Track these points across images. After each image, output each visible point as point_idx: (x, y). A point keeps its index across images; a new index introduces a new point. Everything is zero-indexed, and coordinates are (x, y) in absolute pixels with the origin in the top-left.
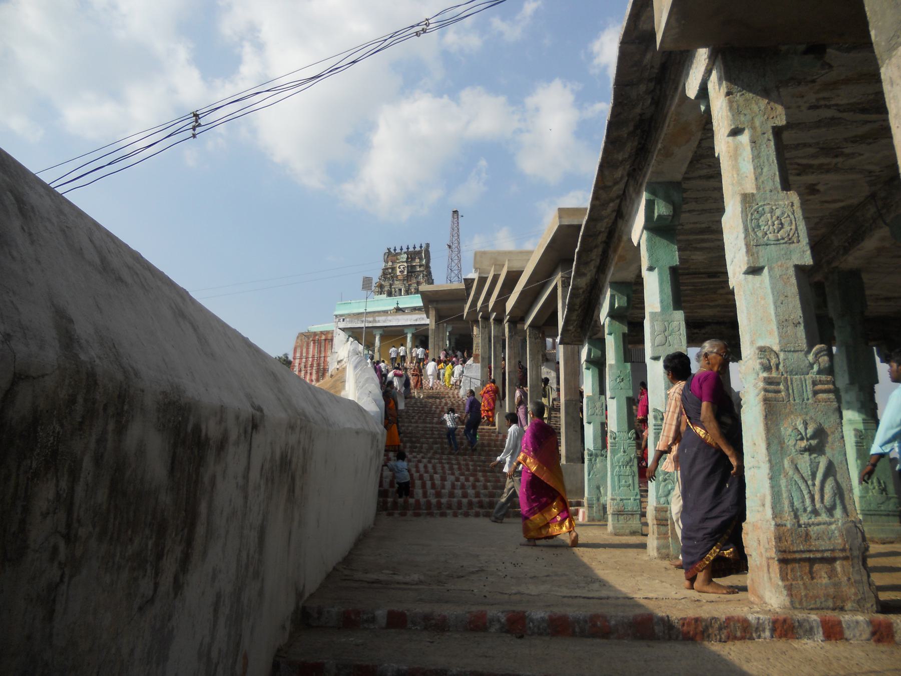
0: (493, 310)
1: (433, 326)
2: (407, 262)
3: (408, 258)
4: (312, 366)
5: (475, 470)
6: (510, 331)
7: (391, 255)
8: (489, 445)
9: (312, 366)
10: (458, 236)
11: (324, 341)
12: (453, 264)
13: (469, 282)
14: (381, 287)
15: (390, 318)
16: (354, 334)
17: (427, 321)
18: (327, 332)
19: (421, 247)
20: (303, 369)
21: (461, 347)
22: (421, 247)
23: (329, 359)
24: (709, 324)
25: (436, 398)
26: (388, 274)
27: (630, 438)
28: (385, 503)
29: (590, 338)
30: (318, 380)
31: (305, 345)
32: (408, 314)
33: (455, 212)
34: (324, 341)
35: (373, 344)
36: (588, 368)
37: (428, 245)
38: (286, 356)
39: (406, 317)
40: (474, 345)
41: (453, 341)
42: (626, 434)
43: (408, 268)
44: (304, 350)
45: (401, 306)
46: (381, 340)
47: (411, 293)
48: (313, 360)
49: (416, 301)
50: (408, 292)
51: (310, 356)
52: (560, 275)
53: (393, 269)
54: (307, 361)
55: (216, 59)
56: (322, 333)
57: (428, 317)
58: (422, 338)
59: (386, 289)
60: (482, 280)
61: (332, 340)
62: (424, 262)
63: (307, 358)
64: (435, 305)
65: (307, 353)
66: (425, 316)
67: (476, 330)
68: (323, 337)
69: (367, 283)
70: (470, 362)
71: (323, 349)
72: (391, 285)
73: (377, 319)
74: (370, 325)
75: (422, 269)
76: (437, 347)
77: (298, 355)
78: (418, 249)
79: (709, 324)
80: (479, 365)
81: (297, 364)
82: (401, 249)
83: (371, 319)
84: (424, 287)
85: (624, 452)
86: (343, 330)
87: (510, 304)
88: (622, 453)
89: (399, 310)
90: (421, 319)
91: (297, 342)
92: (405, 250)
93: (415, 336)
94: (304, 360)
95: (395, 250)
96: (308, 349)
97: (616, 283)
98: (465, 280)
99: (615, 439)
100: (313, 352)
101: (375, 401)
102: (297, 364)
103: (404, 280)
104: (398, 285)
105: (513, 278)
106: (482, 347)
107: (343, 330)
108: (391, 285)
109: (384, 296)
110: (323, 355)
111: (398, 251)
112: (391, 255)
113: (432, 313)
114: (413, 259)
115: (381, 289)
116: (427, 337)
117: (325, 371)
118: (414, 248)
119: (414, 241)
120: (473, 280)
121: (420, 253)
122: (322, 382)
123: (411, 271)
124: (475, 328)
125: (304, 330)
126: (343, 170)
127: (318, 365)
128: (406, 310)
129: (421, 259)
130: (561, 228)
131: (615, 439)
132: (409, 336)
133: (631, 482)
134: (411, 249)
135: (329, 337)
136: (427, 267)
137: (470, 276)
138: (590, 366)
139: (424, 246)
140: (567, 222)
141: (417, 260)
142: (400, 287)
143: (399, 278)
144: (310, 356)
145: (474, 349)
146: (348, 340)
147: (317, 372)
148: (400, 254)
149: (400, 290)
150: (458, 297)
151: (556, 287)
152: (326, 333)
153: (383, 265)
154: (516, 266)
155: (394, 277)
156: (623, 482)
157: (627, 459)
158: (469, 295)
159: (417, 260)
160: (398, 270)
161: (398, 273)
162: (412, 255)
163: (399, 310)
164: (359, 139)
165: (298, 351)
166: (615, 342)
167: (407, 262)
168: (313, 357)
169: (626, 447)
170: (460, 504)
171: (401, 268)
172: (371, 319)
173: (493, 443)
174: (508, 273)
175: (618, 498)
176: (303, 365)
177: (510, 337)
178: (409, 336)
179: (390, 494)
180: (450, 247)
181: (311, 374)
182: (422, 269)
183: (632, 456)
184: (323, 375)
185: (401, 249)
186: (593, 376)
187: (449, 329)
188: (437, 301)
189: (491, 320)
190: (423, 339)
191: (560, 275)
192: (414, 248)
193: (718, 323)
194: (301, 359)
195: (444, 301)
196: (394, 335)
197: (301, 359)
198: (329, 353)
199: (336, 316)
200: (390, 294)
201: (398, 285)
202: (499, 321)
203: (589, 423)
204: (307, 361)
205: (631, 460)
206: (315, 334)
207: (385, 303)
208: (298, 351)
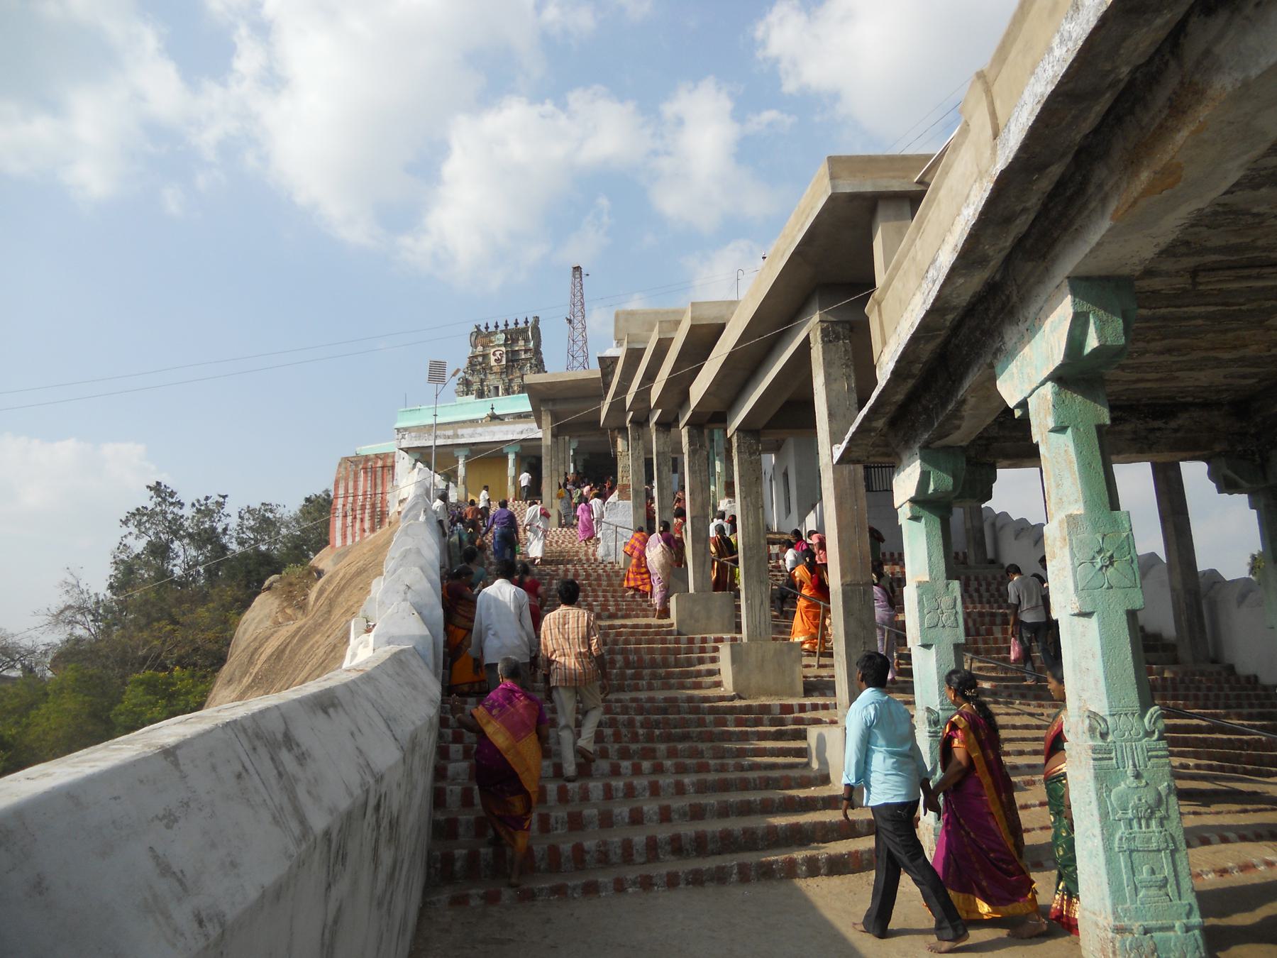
0: (658, 405)
1: (547, 440)
3: (506, 340)
4: (363, 508)
5: (650, 738)
6: (691, 443)
7: (481, 336)
8: (665, 664)
9: (363, 508)
10: (583, 304)
11: (380, 468)
12: (576, 348)
13: (607, 364)
14: (467, 383)
15: (479, 430)
16: (422, 455)
17: (539, 435)
18: (386, 455)
19: (526, 322)
20: (350, 513)
21: (598, 472)
22: (526, 322)
23: (389, 497)
24: (1185, 407)
25: (558, 563)
26: (478, 365)
27: (1149, 734)
28: (448, 860)
29: (925, 447)
30: (373, 530)
31: (352, 476)
32: (508, 423)
33: (577, 269)
34: (380, 468)
35: (455, 472)
36: (915, 518)
37: (537, 319)
38: (327, 492)
39: (505, 428)
40: (620, 470)
41: (580, 463)
42: (1135, 720)
43: (507, 353)
44: (351, 484)
45: (497, 412)
46: (467, 466)
47: (513, 393)
48: (365, 499)
49: (522, 403)
50: (508, 391)
51: (360, 492)
52: (816, 318)
53: (485, 356)
54: (355, 501)
56: (377, 456)
57: (540, 427)
58: (530, 458)
59: (475, 387)
60: (634, 356)
61: (393, 467)
62: (531, 345)
63: (355, 496)
65: (356, 488)
66: (535, 425)
68: (380, 463)
69: (437, 372)
70: (613, 498)
71: (379, 481)
72: (482, 381)
73: (460, 432)
74: (449, 442)
75: (529, 355)
76: (555, 474)
77: (341, 492)
79: (1185, 407)
80: (630, 503)
81: (340, 506)
82: (497, 327)
83: (450, 433)
84: (531, 378)
85: (1138, 776)
86: (407, 450)
87: (698, 390)
88: (1130, 780)
89: (494, 418)
90: (528, 430)
91: (338, 472)
92: (502, 327)
93: (520, 458)
94: (351, 499)
95: (487, 328)
96: (356, 482)
97: (1087, 279)
98: (601, 360)
99: (1104, 736)
100: (365, 486)
101: (420, 610)
102: (340, 506)
104: (493, 380)
105: (703, 338)
106: (635, 472)
107: (407, 450)
108: (482, 381)
109: (471, 398)
110: (379, 491)
111: (492, 329)
112: (481, 336)
113: (547, 420)
114: (515, 341)
116: (539, 459)
117: (384, 514)
118: (516, 324)
119: (516, 314)
120: (615, 360)
121: (525, 331)
122: (379, 531)
123: (513, 360)
124: (620, 441)
125: (351, 454)
126: (402, 216)
127: (373, 506)
128: (508, 418)
129: (526, 340)
130: (833, 199)
131: (1104, 736)
132: (511, 457)
133: (1167, 871)
134: (512, 326)
135: (389, 462)
136: (537, 351)
137: (610, 352)
138: (925, 514)
139: (531, 320)
140: (847, 187)
141: (521, 343)
142: (496, 383)
143: (495, 369)
144: (360, 492)
145: (619, 475)
146: (415, 465)
147: (372, 518)
148: (496, 333)
149: (497, 388)
150: (589, 392)
151: (806, 343)
152: (384, 457)
153: (469, 351)
154: (709, 317)
155: (486, 369)
156: (1144, 873)
157: (1149, 797)
158: (607, 386)
159: (521, 343)
160: (493, 358)
161: (493, 363)
162: (513, 335)
163: (494, 418)
164: (426, 165)
165: (342, 485)
166: (1079, 453)
167: (505, 345)
168: (365, 494)
169: (1140, 760)
170: (627, 846)
171: (496, 355)
172: (450, 433)
173: (671, 658)
174: (693, 328)
175: (1137, 926)
176: (349, 506)
177: (693, 453)
178: (511, 457)
179: (461, 830)
180: (570, 321)
181: (362, 520)
182: (529, 355)
183: (1163, 787)
184: (381, 521)
185: (497, 327)
186: (928, 536)
187: (574, 445)
188: (554, 400)
189: (652, 424)
190: (534, 461)
191: (816, 318)
192: (516, 324)
193: (1206, 405)
194: (346, 497)
195: (565, 400)
196: (487, 458)
197: (346, 497)
198: (388, 488)
199: (398, 430)
200: (481, 395)
201: (493, 380)
202: (667, 425)
203: (926, 646)
204: (355, 501)
205: (1159, 801)
206: (367, 458)
207: (476, 408)
208: (342, 485)
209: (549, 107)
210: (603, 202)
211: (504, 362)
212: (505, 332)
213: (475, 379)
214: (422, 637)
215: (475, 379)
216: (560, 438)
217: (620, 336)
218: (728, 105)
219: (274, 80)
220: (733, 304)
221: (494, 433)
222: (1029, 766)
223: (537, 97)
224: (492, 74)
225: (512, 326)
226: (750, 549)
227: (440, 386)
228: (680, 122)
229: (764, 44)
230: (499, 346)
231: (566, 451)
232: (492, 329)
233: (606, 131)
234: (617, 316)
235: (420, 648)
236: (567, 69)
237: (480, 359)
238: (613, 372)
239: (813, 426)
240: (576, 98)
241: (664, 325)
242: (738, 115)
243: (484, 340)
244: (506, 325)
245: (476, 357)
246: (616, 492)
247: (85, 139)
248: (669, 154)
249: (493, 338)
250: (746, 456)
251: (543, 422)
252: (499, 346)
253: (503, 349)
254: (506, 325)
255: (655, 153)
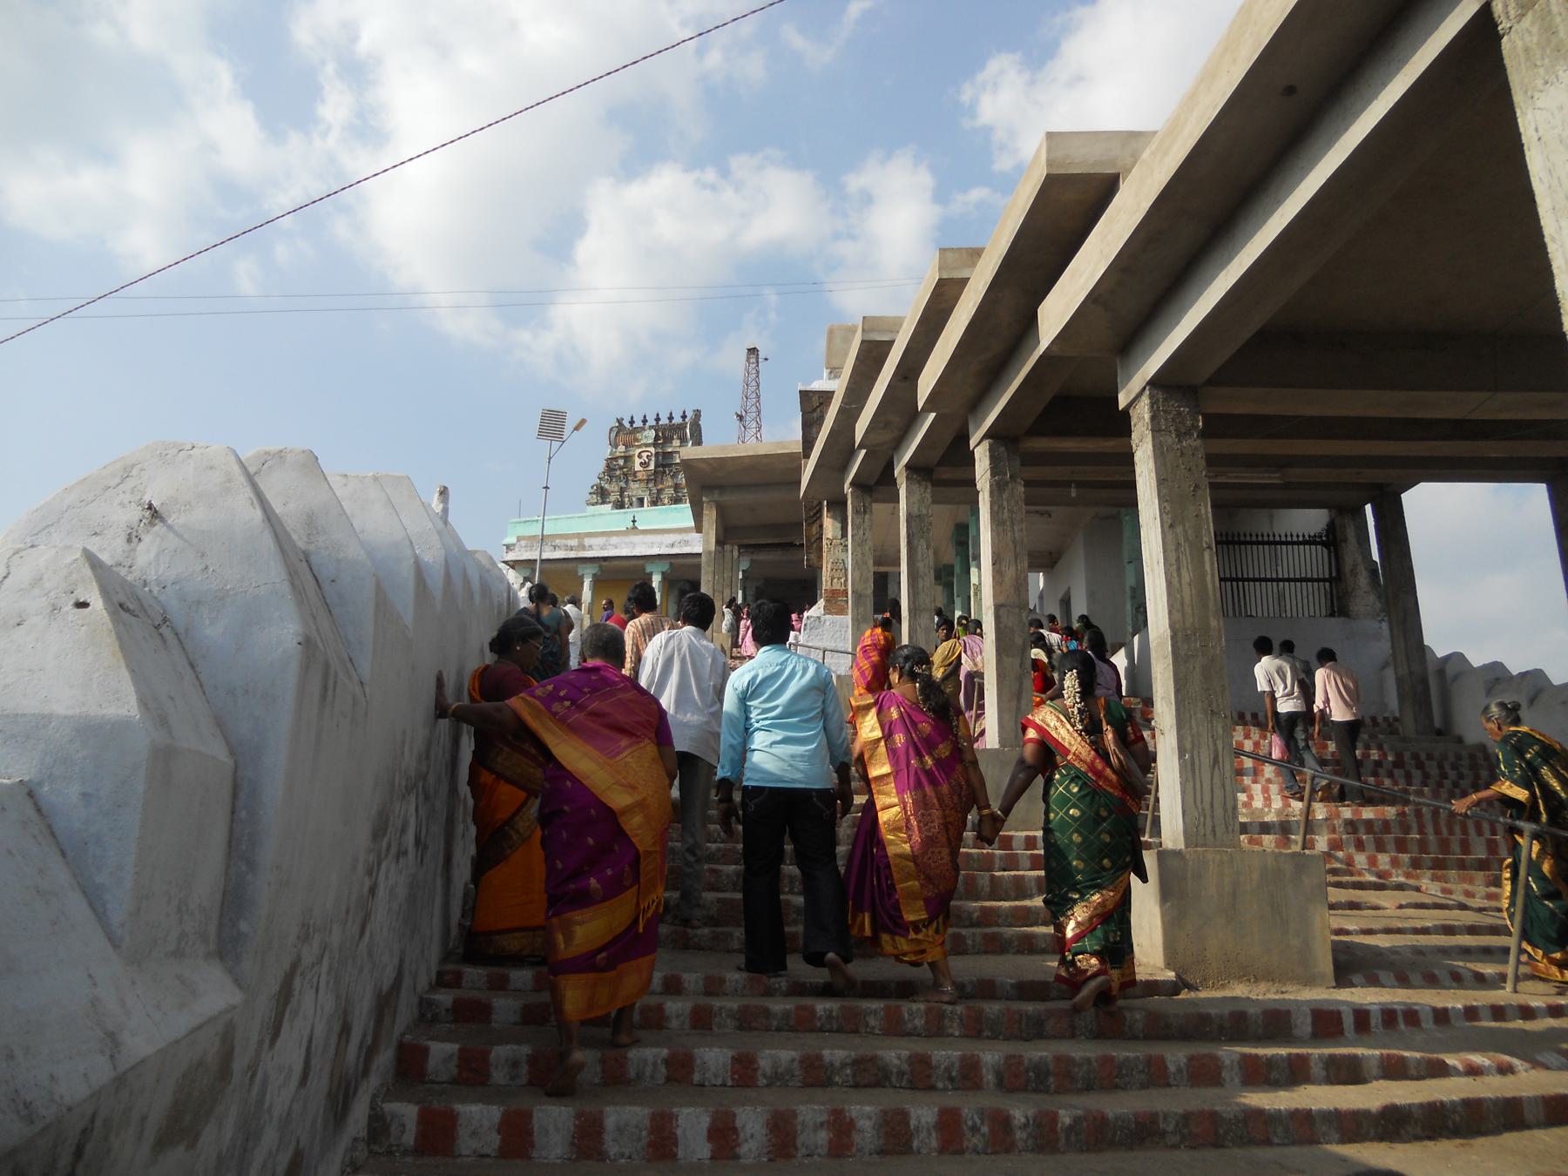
2: (655, 445)
6: (995, 468)
7: (624, 432)
10: (758, 397)
19: (684, 417)
22: (684, 417)
26: (617, 470)
33: (753, 351)
37: (698, 414)
41: (751, 592)
50: (655, 502)
53: (628, 459)
55: (282, 87)
59: (612, 498)
64: (716, 497)
67: (830, 526)
72: (622, 491)
73: (587, 541)
74: (572, 555)
78: (677, 420)
80: (847, 619)
82: (645, 421)
83: (574, 542)
87: (1057, 310)
92: (651, 422)
95: (632, 422)
98: (805, 396)
103: (648, 481)
104: (636, 489)
105: (1066, 207)
108: (622, 491)
111: (638, 424)
112: (624, 432)
114: (668, 440)
115: (602, 495)
118: (671, 418)
119: (670, 404)
120: (827, 396)
121: (681, 427)
126: (523, 305)
134: (664, 421)
139: (690, 415)
142: (640, 494)
143: (640, 475)
148: (643, 429)
153: (607, 451)
154: (1083, 161)
159: (676, 443)
160: (637, 461)
161: (637, 467)
164: (560, 238)
167: (655, 445)
171: (643, 457)
180: (741, 418)
185: (645, 421)
187: (745, 565)
188: (721, 488)
189: (899, 470)
192: (671, 418)
195: (739, 487)
200: (620, 505)
201: (636, 489)
207: (607, 518)
209: (710, 175)
210: (772, 297)
211: (652, 467)
212: (656, 428)
213: (613, 488)
214: (92, 732)
215: (613, 488)
216: (727, 547)
217: (835, 363)
218: (925, 179)
219: (368, 128)
220: (1133, 140)
221: (634, 545)
222: (1389, 1015)
223: (694, 163)
224: (641, 139)
225: (664, 421)
226: (1187, 638)
227: (556, 444)
228: (867, 199)
229: (972, 111)
230: (647, 445)
231: (734, 570)
232: (638, 424)
233: (780, 209)
234: (831, 332)
235: (65, 796)
236: (734, 130)
237: (621, 462)
238: (821, 419)
239: (1133, 504)
240: (740, 164)
241: (949, 255)
242: (941, 196)
243: (630, 438)
244: (658, 419)
245: (616, 459)
246: (821, 603)
247: (133, 195)
248: (853, 237)
249: (639, 436)
250: (1171, 439)
251: (705, 518)
252: (647, 445)
253: (652, 450)
254: (658, 419)
255: (837, 236)
